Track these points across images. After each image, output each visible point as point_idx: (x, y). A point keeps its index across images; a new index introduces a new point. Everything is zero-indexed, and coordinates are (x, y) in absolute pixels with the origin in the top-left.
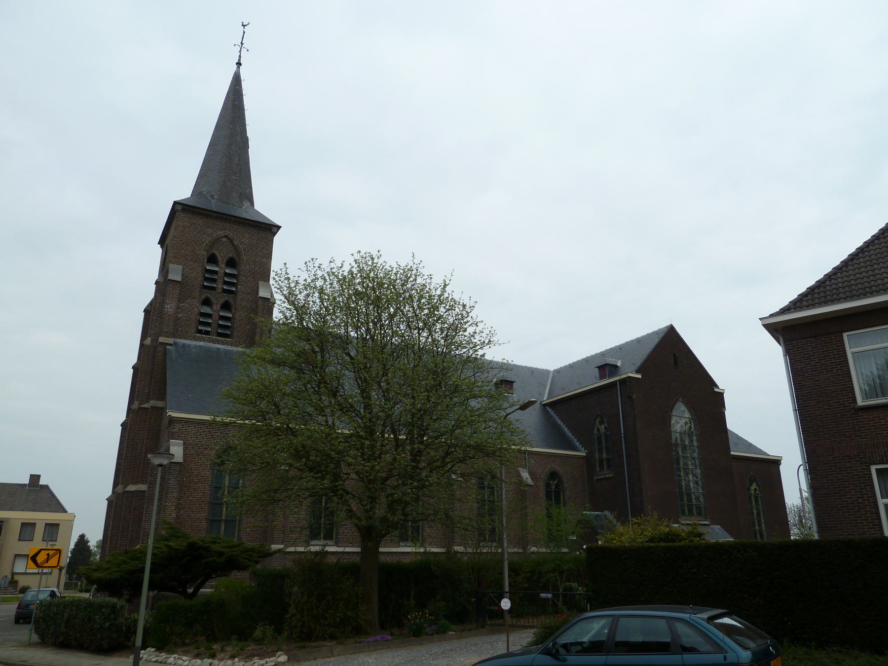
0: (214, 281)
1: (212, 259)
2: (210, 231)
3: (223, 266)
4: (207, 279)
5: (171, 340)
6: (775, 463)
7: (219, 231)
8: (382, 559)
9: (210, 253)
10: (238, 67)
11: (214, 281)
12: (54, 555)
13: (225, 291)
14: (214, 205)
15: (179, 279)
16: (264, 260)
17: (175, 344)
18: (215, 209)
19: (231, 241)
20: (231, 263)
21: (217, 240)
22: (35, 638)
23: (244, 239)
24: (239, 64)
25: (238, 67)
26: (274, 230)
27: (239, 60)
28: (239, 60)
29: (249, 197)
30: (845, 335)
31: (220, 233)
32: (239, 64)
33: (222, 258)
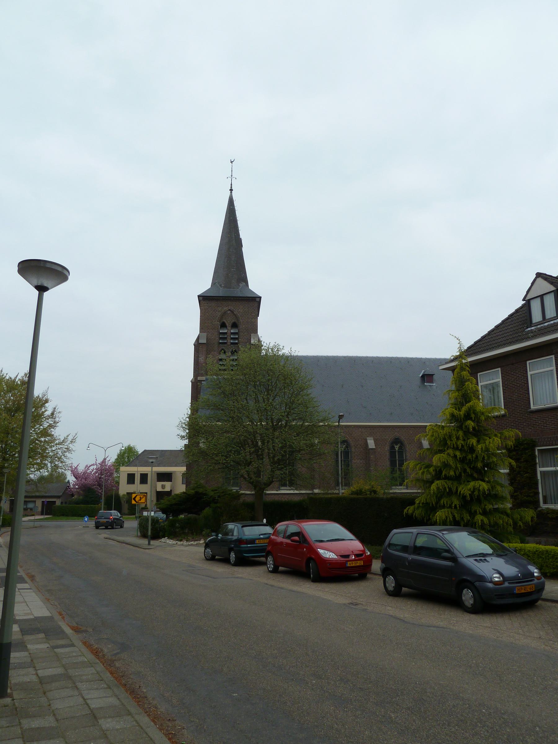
0: (226, 338)
1: (223, 325)
2: (220, 309)
3: (230, 328)
4: (221, 338)
5: (204, 378)
6: (147, 474)
7: (225, 307)
8: (268, 499)
9: (222, 322)
10: (231, 192)
11: (226, 338)
12: (143, 497)
13: (232, 343)
14: (221, 292)
15: (205, 342)
16: (253, 320)
17: (207, 379)
18: (221, 295)
19: (232, 312)
20: (234, 325)
21: (225, 313)
22: (139, 534)
23: (240, 309)
24: (231, 190)
25: (231, 192)
26: (258, 300)
27: (231, 187)
28: (231, 187)
29: (244, 279)
30: (528, 362)
31: (226, 309)
32: (231, 190)
33: (228, 323)
